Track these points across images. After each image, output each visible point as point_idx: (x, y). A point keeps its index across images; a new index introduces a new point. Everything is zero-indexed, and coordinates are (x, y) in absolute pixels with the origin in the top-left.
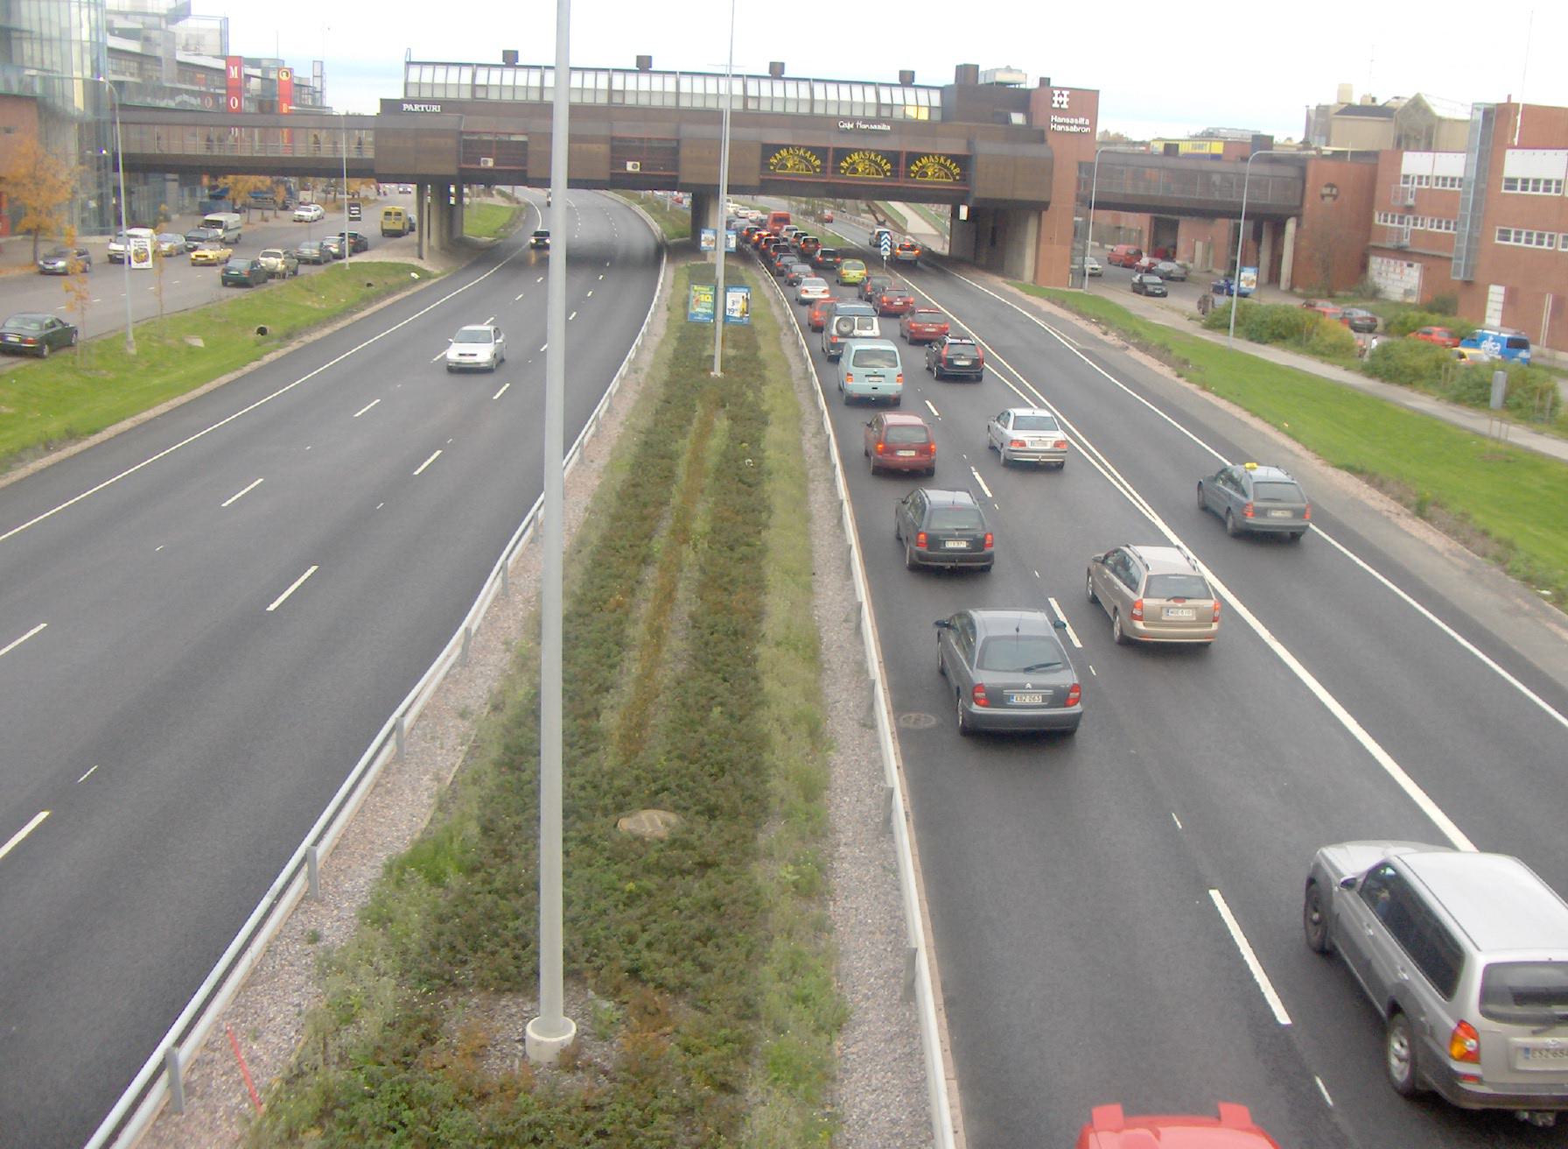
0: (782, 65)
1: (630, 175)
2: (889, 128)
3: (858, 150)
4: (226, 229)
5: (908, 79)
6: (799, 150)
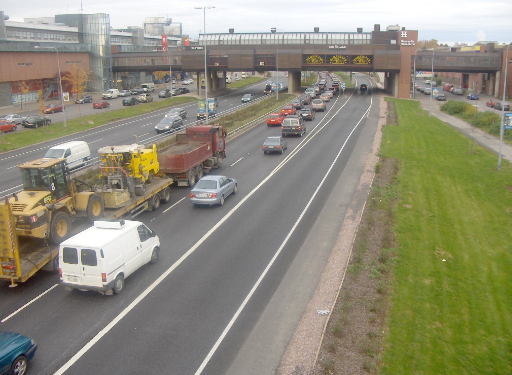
0: (233, 29)
1: (261, 66)
2: (346, 47)
3: (335, 55)
4: (148, 88)
5: (360, 31)
6: (339, 56)
